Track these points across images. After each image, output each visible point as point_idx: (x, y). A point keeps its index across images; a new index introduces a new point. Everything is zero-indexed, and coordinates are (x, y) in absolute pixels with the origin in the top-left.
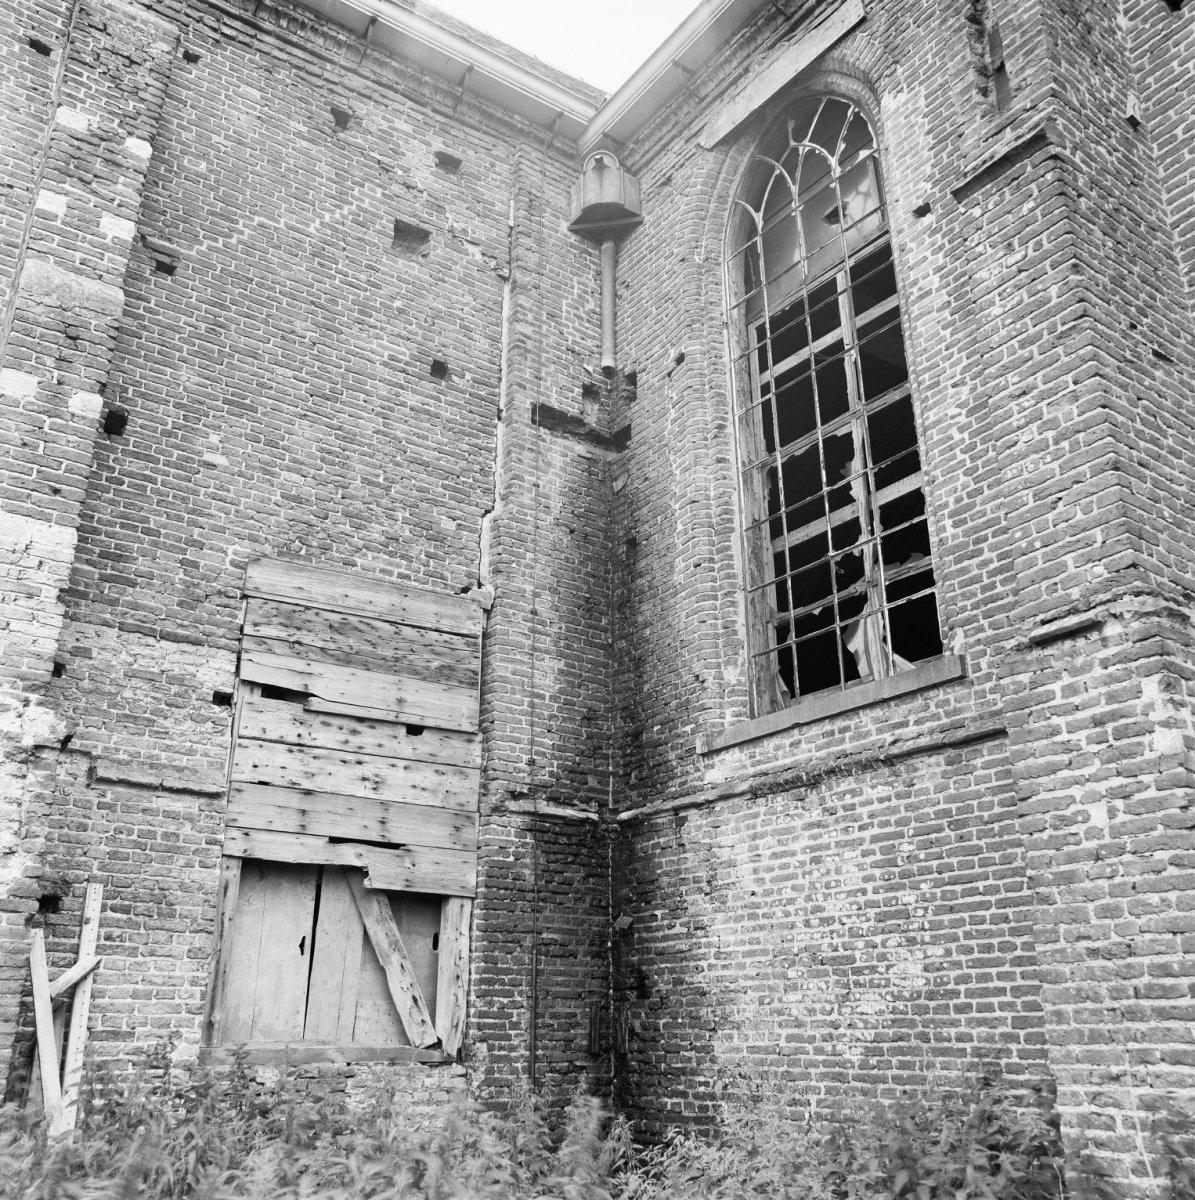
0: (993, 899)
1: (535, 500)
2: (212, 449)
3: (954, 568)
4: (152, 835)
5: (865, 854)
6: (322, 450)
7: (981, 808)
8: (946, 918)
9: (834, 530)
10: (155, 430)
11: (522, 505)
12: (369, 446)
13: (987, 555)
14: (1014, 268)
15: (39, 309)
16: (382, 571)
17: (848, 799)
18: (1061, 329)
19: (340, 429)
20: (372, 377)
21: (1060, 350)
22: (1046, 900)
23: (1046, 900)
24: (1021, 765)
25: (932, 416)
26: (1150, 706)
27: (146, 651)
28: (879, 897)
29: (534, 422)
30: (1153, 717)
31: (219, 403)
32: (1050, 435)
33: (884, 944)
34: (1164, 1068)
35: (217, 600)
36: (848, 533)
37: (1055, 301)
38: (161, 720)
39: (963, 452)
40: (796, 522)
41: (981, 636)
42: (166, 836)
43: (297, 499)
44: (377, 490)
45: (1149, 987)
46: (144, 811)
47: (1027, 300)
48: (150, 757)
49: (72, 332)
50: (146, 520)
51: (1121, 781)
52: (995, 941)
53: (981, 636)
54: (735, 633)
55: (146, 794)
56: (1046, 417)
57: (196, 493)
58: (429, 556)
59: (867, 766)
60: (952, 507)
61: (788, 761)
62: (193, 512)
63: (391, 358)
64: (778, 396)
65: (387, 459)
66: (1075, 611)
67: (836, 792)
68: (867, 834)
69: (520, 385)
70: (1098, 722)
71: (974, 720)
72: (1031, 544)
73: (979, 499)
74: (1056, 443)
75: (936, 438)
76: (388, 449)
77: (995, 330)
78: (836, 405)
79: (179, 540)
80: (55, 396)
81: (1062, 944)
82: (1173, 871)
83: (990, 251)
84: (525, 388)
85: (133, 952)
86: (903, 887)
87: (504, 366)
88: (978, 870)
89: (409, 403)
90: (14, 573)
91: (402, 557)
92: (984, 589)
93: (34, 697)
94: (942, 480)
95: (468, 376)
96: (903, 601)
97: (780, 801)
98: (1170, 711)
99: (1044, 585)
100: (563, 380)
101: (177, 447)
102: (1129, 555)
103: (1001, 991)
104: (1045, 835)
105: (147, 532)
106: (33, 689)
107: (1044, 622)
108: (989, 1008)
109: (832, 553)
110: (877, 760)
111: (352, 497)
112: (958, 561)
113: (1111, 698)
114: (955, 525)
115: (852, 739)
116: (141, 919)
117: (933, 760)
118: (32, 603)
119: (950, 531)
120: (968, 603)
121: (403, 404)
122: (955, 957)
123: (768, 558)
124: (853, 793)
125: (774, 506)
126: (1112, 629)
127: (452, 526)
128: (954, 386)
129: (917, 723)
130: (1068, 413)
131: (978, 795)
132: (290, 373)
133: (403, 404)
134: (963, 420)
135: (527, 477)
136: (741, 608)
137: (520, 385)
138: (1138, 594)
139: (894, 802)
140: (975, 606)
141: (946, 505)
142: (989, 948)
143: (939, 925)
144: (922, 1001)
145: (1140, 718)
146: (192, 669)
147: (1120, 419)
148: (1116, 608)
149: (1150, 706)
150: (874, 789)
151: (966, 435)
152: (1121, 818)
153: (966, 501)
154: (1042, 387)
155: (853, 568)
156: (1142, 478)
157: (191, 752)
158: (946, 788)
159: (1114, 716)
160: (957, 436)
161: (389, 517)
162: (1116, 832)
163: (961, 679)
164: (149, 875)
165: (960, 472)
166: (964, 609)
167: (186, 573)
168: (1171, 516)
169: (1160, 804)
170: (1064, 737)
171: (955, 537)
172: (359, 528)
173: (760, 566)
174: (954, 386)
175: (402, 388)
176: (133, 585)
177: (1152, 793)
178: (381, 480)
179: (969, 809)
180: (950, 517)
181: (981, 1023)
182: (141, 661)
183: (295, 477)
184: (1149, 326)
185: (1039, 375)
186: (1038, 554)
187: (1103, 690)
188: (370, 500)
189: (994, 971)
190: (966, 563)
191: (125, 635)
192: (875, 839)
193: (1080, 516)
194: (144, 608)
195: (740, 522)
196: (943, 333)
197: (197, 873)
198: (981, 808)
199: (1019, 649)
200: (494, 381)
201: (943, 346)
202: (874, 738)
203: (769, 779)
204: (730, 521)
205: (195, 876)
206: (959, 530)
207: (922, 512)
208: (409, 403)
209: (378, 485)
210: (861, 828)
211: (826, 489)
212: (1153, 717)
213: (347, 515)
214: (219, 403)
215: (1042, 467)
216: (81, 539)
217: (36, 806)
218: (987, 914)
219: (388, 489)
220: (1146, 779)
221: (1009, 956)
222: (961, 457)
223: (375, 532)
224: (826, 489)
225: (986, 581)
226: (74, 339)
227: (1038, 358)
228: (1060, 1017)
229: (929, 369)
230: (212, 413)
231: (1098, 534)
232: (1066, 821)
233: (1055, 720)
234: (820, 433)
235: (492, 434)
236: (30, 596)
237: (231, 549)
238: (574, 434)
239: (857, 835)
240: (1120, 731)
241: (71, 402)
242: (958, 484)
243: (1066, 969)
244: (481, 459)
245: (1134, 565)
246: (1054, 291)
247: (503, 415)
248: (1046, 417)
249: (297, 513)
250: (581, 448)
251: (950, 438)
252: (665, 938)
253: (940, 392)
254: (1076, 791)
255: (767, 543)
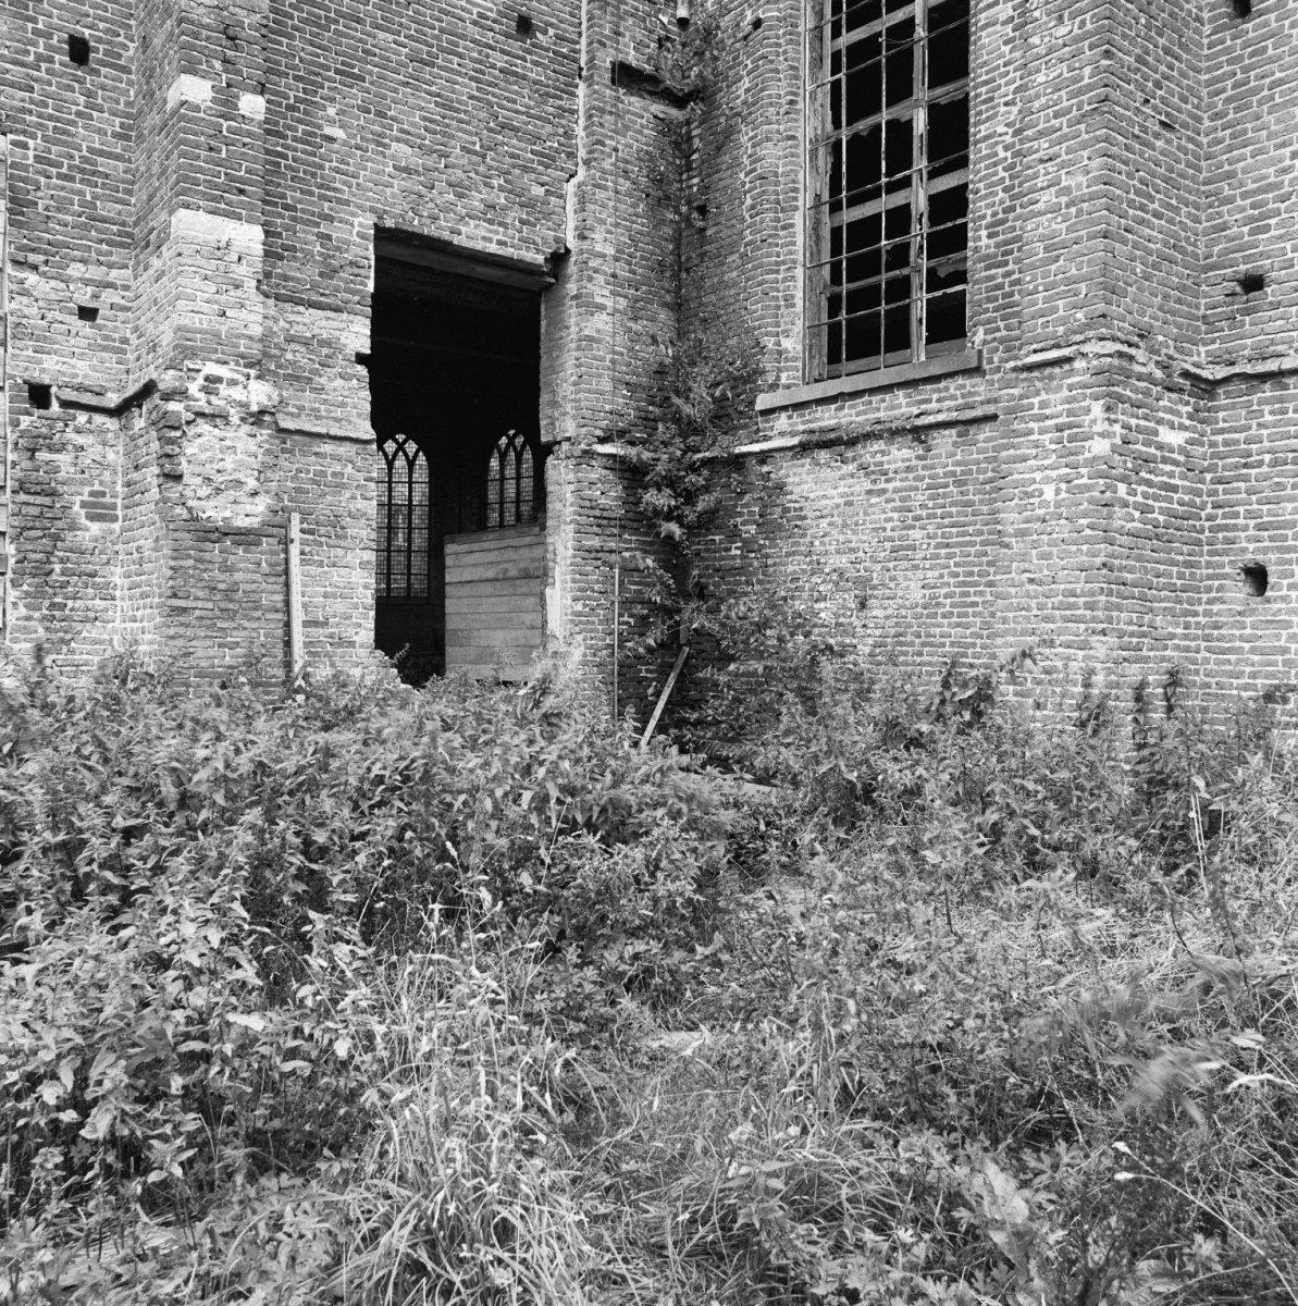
0: (978, 539)
1: (614, 165)
2: (332, 122)
3: (984, 274)
4: (323, 474)
5: (887, 501)
6: (425, 119)
7: (978, 472)
8: (943, 551)
9: (880, 16)
10: (280, 105)
11: (604, 172)
12: (465, 112)
13: (1011, 267)
14: (1061, 41)
15: (202, 10)
16: (484, 238)
17: (879, 458)
18: (1087, 108)
19: (438, 95)
20: (463, 37)
21: (1082, 127)
22: (1007, 546)
23: (1007, 546)
24: (1004, 454)
25: (983, 130)
26: (1094, 421)
27: (298, 318)
28: (896, 534)
29: (613, 82)
30: (1095, 429)
31: (331, 74)
32: (1064, 200)
33: (895, 568)
34: (1061, 650)
35: (348, 269)
36: (900, 219)
37: (1086, 81)
38: (317, 378)
39: (1005, 169)
40: (852, 202)
41: (998, 335)
42: (334, 474)
43: (406, 170)
44: (475, 159)
45: (1061, 603)
46: (316, 454)
47: (1066, 75)
48: (313, 410)
49: (231, 32)
50: (283, 196)
51: (1068, 470)
52: (976, 569)
53: (998, 335)
54: (794, 305)
55: (317, 441)
56: (1063, 184)
57: (322, 167)
58: (522, 222)
59: (895, 433)
60: (989, 219)
61: (833, 422)
62: (321, 187)
63: (480, 15)
64: (847, 75)
65: (482, 125)
66: (1057, 346)
67: (870, 452)
68: (890, 486)
69: (600, 42)
70: (1059, 429)
71: (982, 403)
72: (1036, 287)
73: (1011, 216)
74: (1067, 206)
75: (984, 152)
76: (483, 115)
77: (1037, 96)
78: (901, 91)
79: (313, 214)
80: (226, 102)
81: (1013, 575)
82: (1088, 532)
83: (1045, 18)
84: (604, 45)
85: (321, 564)
86: (914, 527)
87: (584, 19)
88: (970, 518)
89: (499, 65)
90: (222, 268)
91: (500, 224)
92: (1005, 296)
93: (253, 372)
94: (984, 176)
95: (551, 32)
96: (939, 293)
97: (823, 455)
98: (1106, 426)
99: (1041, 320)
100: (640, 34)
101: (300, 121)
102: (1101, 307)
103: (975, 604)
104: (1013, 503)
105: (286, 207)
106: (249, 365)
107: (1035, 351)
108: (966, 615)
109: (884, 242)
110: (904, 429)
111: (453, 167)
112: (987, 268)
113: (1070, 413)
114: (990, 236)
115: (886, 409)
116: (323, 539)
117: (947, 432)
118: (239, 293)
119: (985, 241)
120: (991, 306)
121: (493, 67)
122: (946, 579)
123: (826, 233)
124: (883, 453)
125: (835, 188)
126: (1079, 364)
127: (541, 191)
128: (1006, 104)
129: (938, 401)
130: (1077, 182)
131: (978, 462)
132: (391, 37)
133: (493, 67)
134: (1008, 139)
135: (608, 142)
136: (800, 284)
137: (600, 42)
138: (1101, 339)
139: (914, 462)
140: (996, 310)
141: (984, 217)
142: (971, 574)
143: (937, 557)
144: (919, 610)
145: (1086, 429)
146: (337, 333)
147: (1118, 192)
148: (1086, 348)
149: (1094, 421)
150: (900, 454)
151: (1009, 154)
152: (1063, 495)
153: (1001, 216)
154: (1064, 157)
155: (900, 256)
156: (1124, 242)
157: (343, 405)
158: (955, 454)
159: (1070, 426)
160: (1002, 154)
161: (487, 185)
162: (1058, 505)
163: (977, 371)
164: (322, 509)
165: (1000, 188)
166: (987, 311)
167: (322, 245)
168: (1143, 271)
169: (1088, 488)
170: (1035, 437)
171: (988, 247)
172: (461, 196)
173: (818, 239)
174: (1006, 104)
175: (491, 48)
176: (281, 258)
177: (1085, 480)
178: (477, 148)
179: (970, 472)
180: (987, 228)
181: (959, 625)
182: (296, 327)
183: (404, 147)
184: (1162, 98)
185: (1064, 145)
186: (1040, 296)
187: (1066, 406)
188: (469, 168)
189: (972, 590)
190: (993, 271)
191: (281, 304)
192: (896, 491)
193: (1074, 271)
194: (292, 279)
195: (804, 201)
196: (1003, 48)
197: (360, 504)
198: (978, 472)
199: (1015, 369)
200: (575, 37)
201: (1001, 62)
202: (903, 410)
203: (815, 438)
204: (796, 199)
205: (359, 506)
206: (992, 241)
207: (964, 215)
208: (499, 65)
209: (476, 153)
210: (887, 481)
211: (884, 180)
212: (1095, 429)
213: (450, 185)
214: (331, 74)
215: (1054, 226)
216: (267, 233)
217: (267, 459)
218: (973, 550)
219: (484, 156)
220: (1083, 471)
221: (984, 580)
222: (1002, 174)
223: (476, 201)
224: (884, 180)
225: (1007, 289)
226: (232, 39)
227: (1066, 130)
228: (1005, 620)
229: (986, 83)
230: (327, 84)
231: (1083, 288)
232: (1028, 495)
233: (1032, 424)
234: (884, 116)
235: (573, 95)
236: (237, 287)
237: (356, 221)
238: (651, 93)
239: (883, 486)
240: (1071, 433)
241: (240, 105)
242: (997, 199)
243: (1013, 590)
244: (564, 122)
245: (1104, 316)
246: (1087, 71)
247: (584, 73)
248: (1063, 184)
249: (407, 184)
250: (657, 108)
251: (996, 154)
252: (722, 558)
253: (993, 108)
254: (1038, 476)
255: (826, 218)
